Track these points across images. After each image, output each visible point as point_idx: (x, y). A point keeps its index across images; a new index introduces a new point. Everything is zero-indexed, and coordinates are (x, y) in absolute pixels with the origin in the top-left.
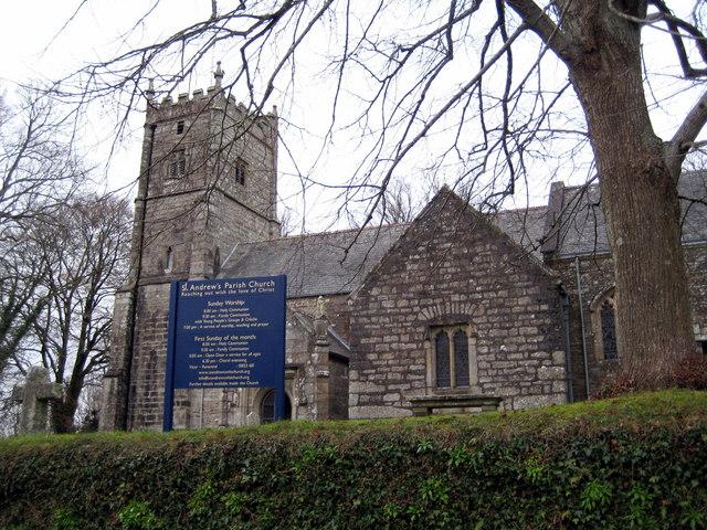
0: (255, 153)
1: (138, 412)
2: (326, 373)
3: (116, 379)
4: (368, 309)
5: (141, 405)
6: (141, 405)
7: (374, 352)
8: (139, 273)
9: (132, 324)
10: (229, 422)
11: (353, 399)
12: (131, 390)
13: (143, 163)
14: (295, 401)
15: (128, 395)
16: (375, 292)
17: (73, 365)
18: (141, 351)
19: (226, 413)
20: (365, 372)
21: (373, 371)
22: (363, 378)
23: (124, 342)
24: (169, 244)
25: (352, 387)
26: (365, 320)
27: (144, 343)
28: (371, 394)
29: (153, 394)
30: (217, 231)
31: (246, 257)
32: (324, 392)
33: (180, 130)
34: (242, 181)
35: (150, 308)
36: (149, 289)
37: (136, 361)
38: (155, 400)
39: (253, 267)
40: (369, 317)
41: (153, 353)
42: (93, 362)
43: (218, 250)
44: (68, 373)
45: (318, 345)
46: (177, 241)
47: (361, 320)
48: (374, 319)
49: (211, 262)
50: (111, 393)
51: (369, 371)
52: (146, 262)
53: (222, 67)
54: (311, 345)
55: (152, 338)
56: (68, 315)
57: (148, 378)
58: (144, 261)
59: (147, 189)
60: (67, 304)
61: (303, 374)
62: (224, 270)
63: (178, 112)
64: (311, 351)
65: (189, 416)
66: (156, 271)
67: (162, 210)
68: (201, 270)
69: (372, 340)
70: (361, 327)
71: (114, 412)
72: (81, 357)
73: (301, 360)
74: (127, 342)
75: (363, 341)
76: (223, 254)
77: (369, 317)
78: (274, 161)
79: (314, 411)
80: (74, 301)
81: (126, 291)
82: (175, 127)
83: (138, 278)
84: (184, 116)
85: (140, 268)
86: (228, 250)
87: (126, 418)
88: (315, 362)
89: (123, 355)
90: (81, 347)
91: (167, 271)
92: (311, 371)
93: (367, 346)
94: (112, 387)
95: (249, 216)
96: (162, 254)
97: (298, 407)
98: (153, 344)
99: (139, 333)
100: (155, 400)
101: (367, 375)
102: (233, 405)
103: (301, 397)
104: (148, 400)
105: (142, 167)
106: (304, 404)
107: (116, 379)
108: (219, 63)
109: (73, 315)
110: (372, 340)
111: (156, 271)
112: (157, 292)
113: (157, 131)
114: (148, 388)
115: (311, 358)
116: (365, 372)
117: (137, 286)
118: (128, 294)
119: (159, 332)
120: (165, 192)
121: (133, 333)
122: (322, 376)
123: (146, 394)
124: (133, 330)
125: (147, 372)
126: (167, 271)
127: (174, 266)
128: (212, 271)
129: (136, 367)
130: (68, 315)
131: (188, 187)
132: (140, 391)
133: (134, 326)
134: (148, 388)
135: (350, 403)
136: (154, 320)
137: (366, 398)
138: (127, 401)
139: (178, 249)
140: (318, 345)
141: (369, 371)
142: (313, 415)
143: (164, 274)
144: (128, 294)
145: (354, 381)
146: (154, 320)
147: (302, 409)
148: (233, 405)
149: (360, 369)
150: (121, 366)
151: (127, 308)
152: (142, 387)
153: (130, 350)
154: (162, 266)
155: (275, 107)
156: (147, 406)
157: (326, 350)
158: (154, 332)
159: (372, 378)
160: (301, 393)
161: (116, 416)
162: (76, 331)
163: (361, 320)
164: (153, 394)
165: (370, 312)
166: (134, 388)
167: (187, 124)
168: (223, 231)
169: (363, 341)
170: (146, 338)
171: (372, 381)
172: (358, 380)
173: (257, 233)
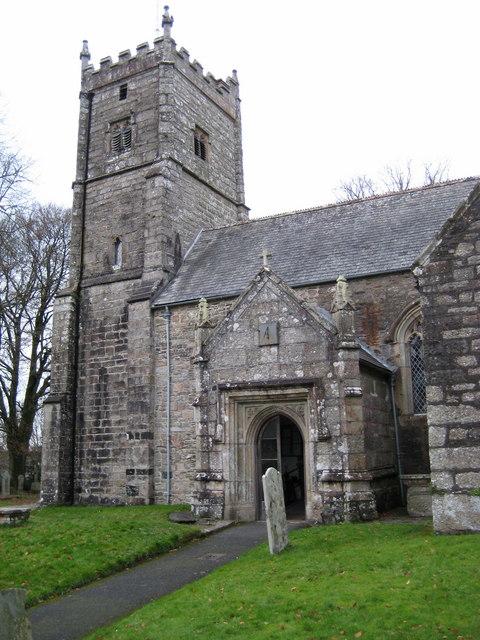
0: (214, 121)
1: (88, 446)
2: (357, 390)
3: (58, 406)
4: (452, 280)
5: (91, 438)
6: (91, 438)
7: (469, 353)
8: (82, 274)
9: (75, 336)
10: (212, 467)
11: (436, 436)
12: (78, 419)
13: (80, 139)
14: (310, 434)
15: (74, 425)
16: (461, 251)
17: (306, 446)
18: (88, 370)
19: (207, 452)
20: (456, 388)
21: (472, 386)
22: (452, 398)
23: (67, 359)
24: (117, 233)
25: (433, 415)
26: (449, 299)
27: (91, 360)
28: (467, 426)
29: (105, 423)
30: (176, 214)
31: (215, 245)
32: (357, 420)
33: (123, 94)
34: (203, 157)
35: (96, 313)
36: (93, 291)
37: (83, 382)
38: (108, 430)
39: (225, 255)
40: (454, 293)
41: (103, 371)
42: (46, 384)
43: (178, 236)
44: (21, 397)
45: (344, 348)
46: (126, 229)
47: (440, 300)
48: (463, 297)
49: (170, 251)
50: (53, 423)
51: (463, 387)
52: (89, 259)
53: (171, 13)
54: (333, 349)
55: (101, 352)
56: (18, 335)
57: (98, 402)
58: (87, 258)
59: (87, 171)
60: (17, 324)
61: (322, 394)
62: (187, 262)
63: (120, 73)
64: (332, 358)
65: (152, 453)
66: (102, 269)
67: (102, 192)
68: (158, 262)
69: (465, 333)
70: (442, 312)
71: (57, 447)
72: (34, 379)
73: (317, 372)
74: (70, 360)
75: (447, 335)
76: (184, 243)
77: (454, 293)
78: (237, 135)
79: (343, 448)
80: (24, 320)
81: (66, 296)
82: (117, 92)
83: (81, 279)
84: (127, 78)
85: (82, 267)
86: (191, 238)
87: (73, 454)
88: (341, 374)
89: (65, 376)
90: (33, 368)
91: (116, 268)
92: (333, 388)
93: (455, 343)
94: (54, 416)
95: (213, 196)
96: (108, 247)
97: (316, 443)
98: (102, 360)
99: (84, 347)
100: (108, 430)
101: (459, 393)
102: (216, 442)
103: (321, 427)
104: (99, 431)
105: (79, 145)
106: (325, 439)
107: (58, 406)
108: (166, 8)
109: (23, 335)
110: (465, 333)
111: (102, 269)
112: (104, 294)
113: (96, 100)
114: (98, 415)
115: (333, 369)
116: (456, 388)
117: (79, 288)
118: (69, 299)
119: (109, 344)
120: (108, 171)
121: (77, 347)
122: (352, 396)
123: (97, 424)
124: (77, 342)
125: (97, 395)
126: (116, 268)
127: (124, 261)
128: (171, 264)
129: (83, 389)
130: (18, 335)
131: (134, 162)
132: (89, 420)
133: (77, 338)
134: (98, 415)
135: (431, 442)
136: (102, 330)
137: (461, 433)
138: (74, 432)
139: (127, 239)
140: (344, 348)
141: (463, 387)
142: (342, 455)
143: (112, 272)
144: (69, 299)
145: (435, 404)
146: (102, 330)
147: (324, 447)
148: (216, 442)
149: (446, 384)
150: (64, 389)
151: (68, 316)
152: (91, 414)
153: (75, 369)
154: (109, 261)
155: (235, 71)
156: (98, 438)
157: (355, 355)
158: (103, 344)
159: (468, 397)
160: (320, 422)
161: (61, 452)
162: (27, 351)
163: (440, 300)
164: (105, 423)
165: (456, 285)
166: (82, 415)
167: (131, 86)
168: (183, 214)
169: (447, 335)
170: (93, 353)
171: (471, 403)
172: (444, 402)
173: (227, 217)
